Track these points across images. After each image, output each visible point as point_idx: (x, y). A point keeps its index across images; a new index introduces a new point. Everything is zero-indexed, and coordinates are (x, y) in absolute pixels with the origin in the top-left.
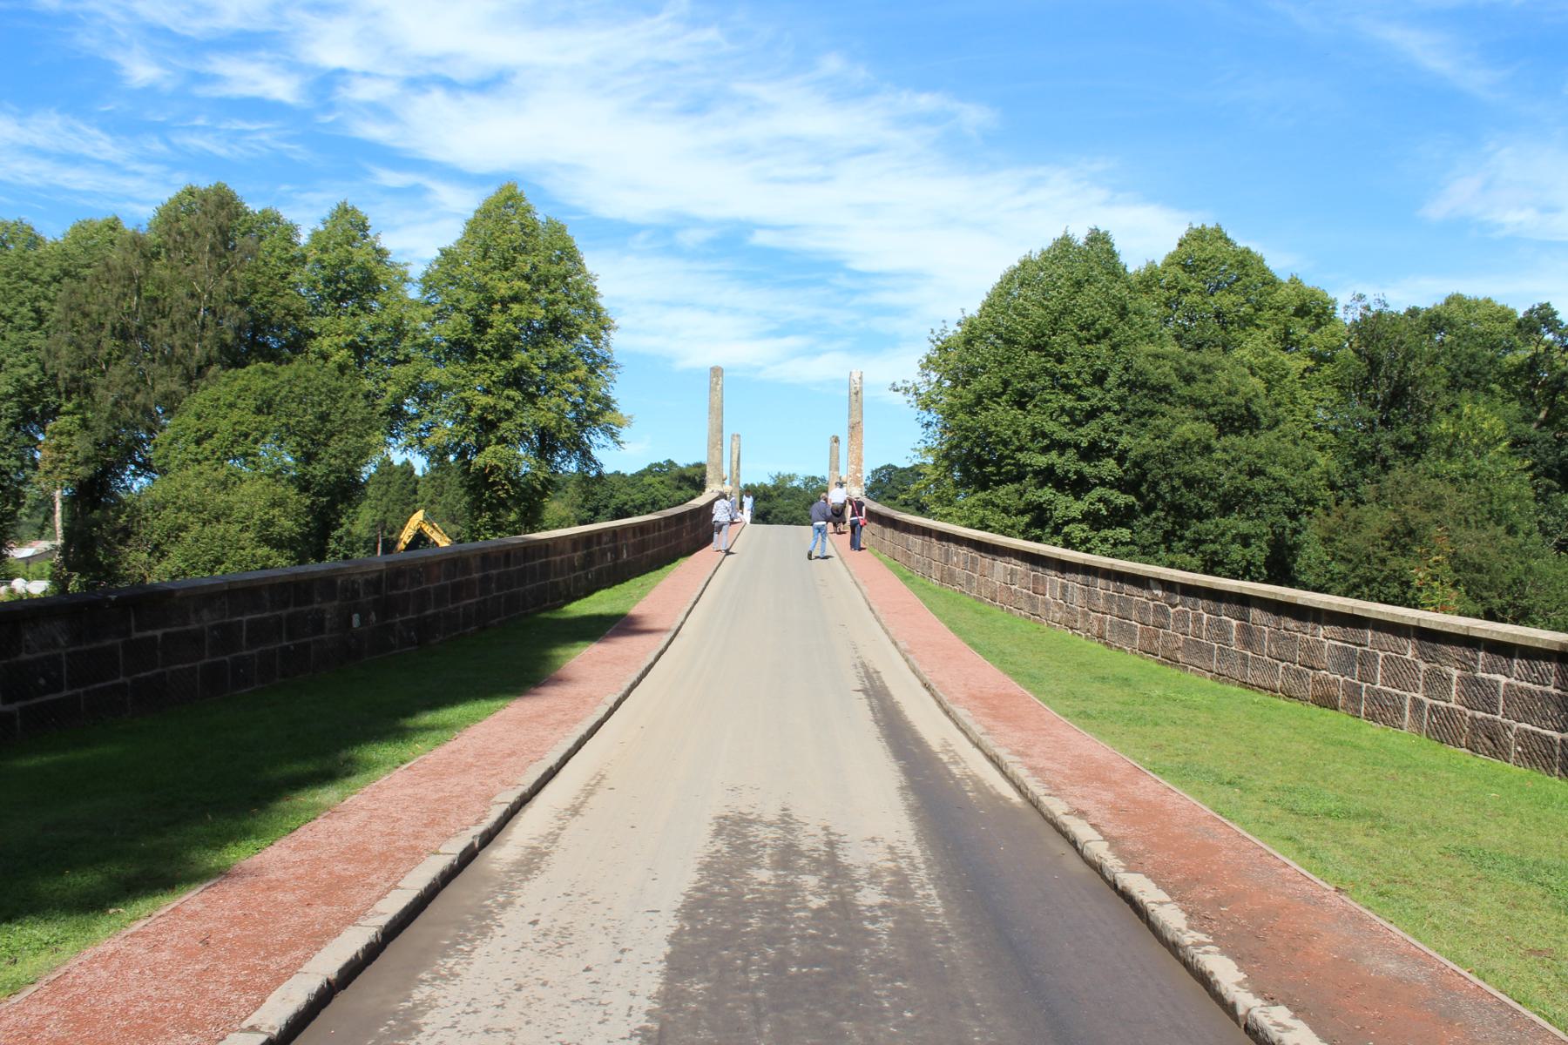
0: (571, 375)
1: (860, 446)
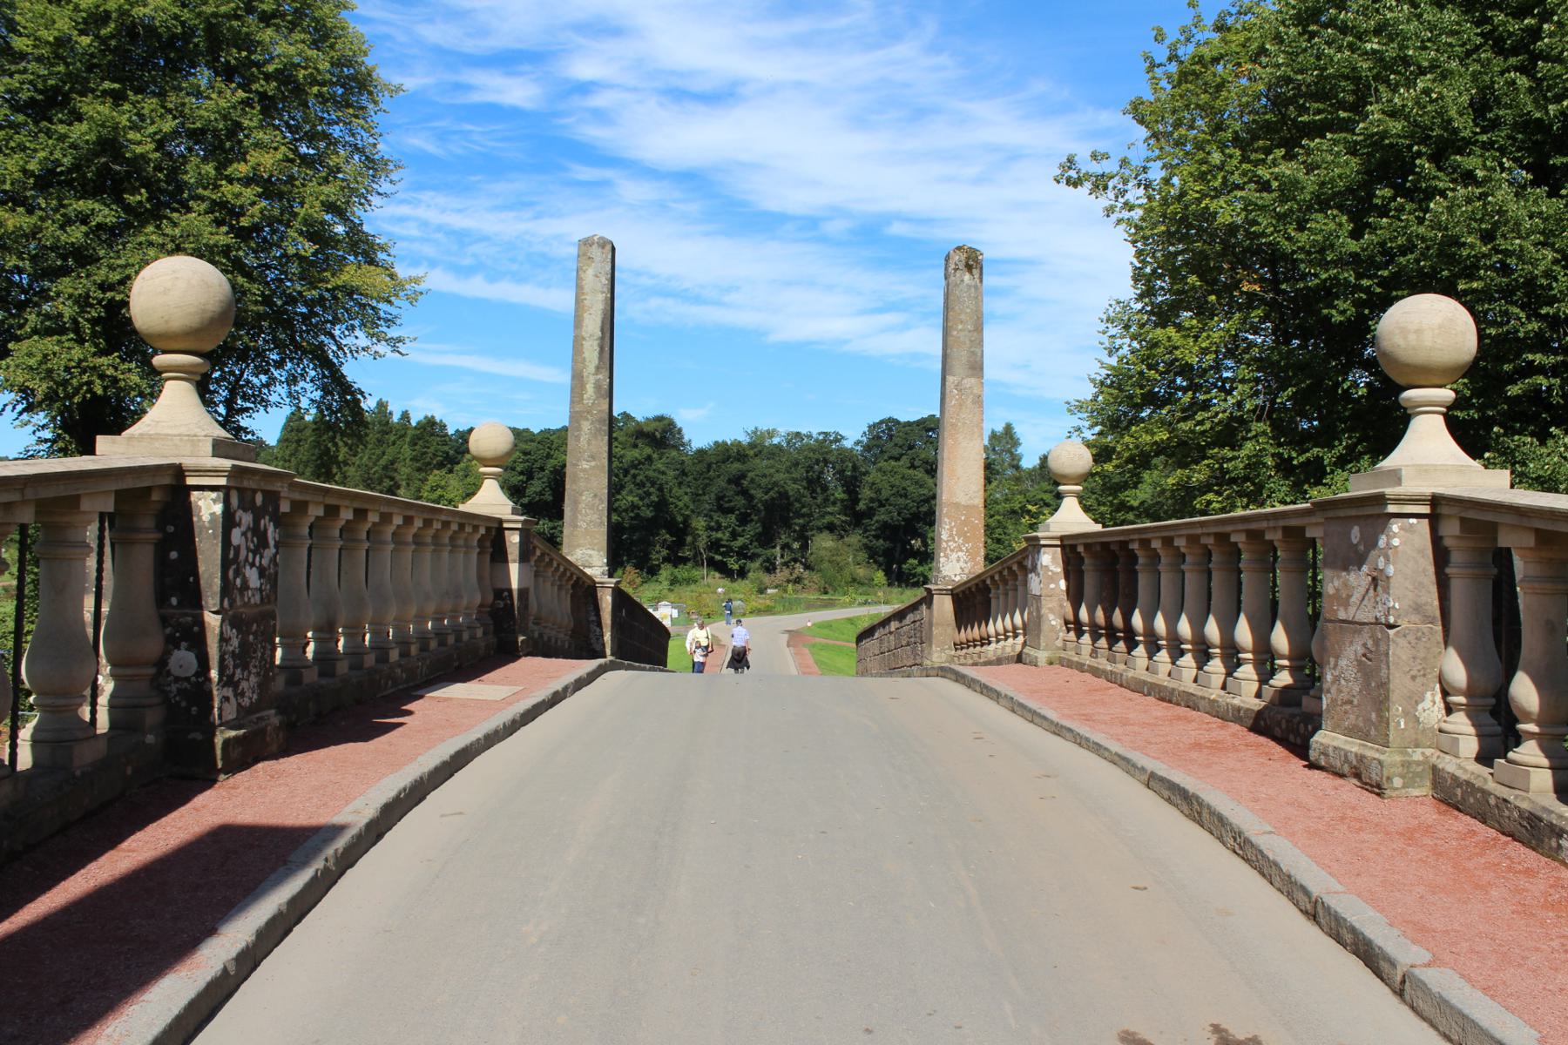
0: (242, 169)
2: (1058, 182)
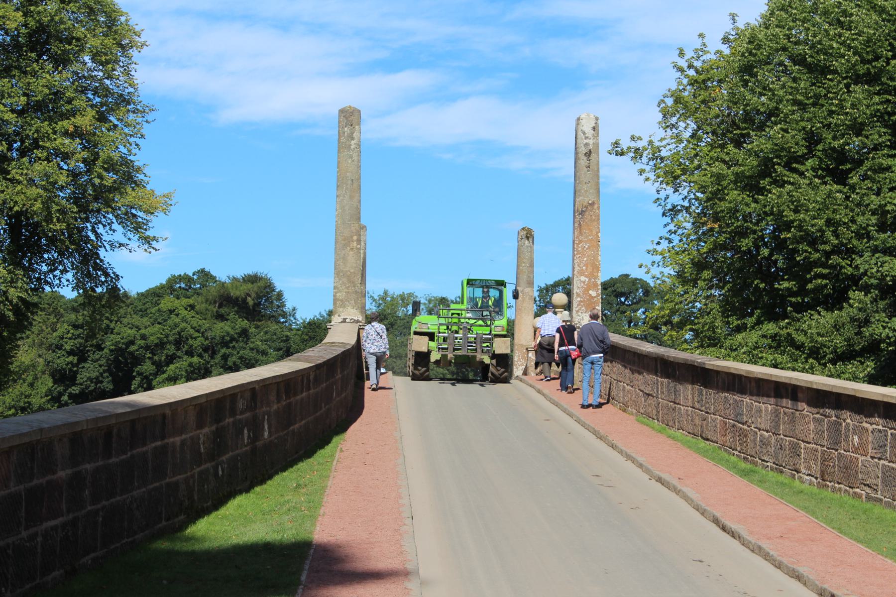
1: (596, 243)
2: (611, 154)
